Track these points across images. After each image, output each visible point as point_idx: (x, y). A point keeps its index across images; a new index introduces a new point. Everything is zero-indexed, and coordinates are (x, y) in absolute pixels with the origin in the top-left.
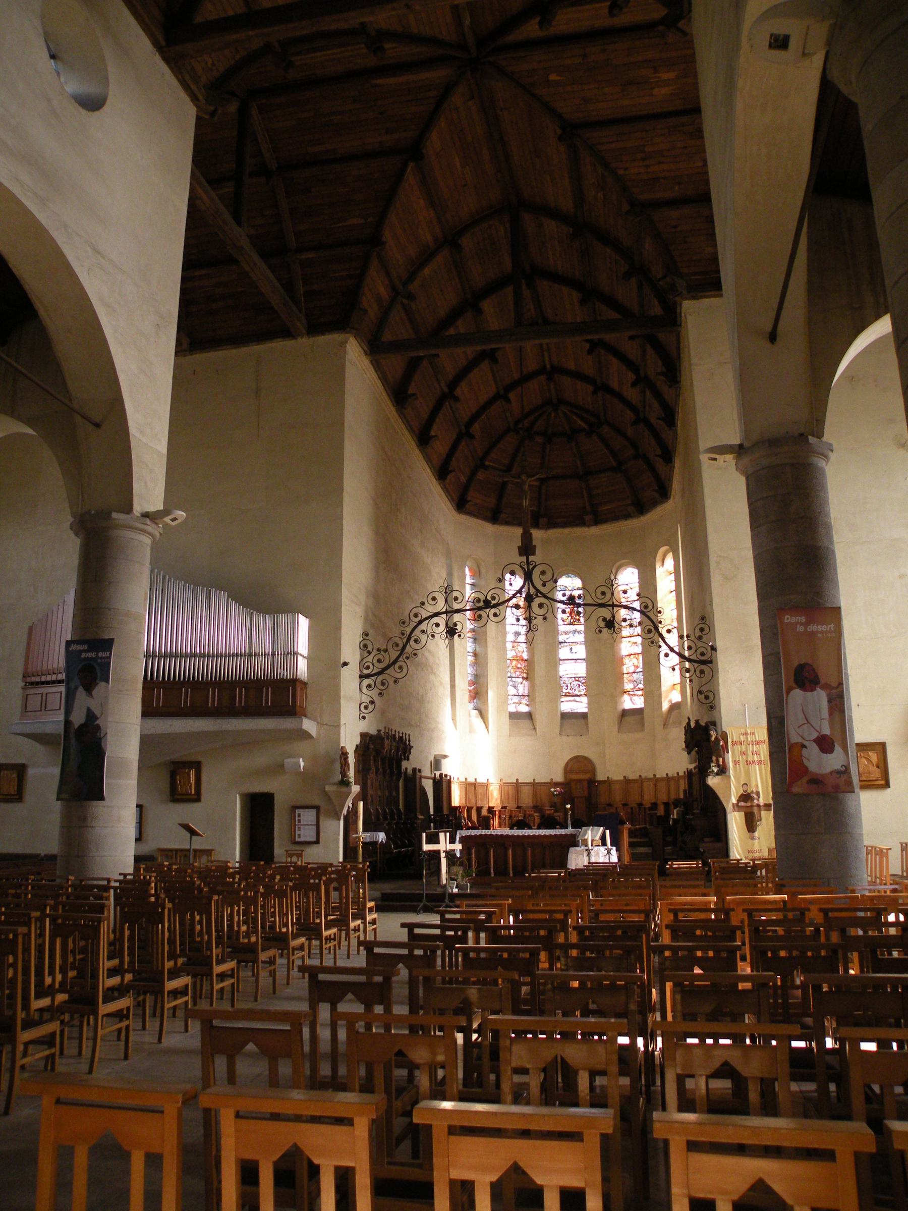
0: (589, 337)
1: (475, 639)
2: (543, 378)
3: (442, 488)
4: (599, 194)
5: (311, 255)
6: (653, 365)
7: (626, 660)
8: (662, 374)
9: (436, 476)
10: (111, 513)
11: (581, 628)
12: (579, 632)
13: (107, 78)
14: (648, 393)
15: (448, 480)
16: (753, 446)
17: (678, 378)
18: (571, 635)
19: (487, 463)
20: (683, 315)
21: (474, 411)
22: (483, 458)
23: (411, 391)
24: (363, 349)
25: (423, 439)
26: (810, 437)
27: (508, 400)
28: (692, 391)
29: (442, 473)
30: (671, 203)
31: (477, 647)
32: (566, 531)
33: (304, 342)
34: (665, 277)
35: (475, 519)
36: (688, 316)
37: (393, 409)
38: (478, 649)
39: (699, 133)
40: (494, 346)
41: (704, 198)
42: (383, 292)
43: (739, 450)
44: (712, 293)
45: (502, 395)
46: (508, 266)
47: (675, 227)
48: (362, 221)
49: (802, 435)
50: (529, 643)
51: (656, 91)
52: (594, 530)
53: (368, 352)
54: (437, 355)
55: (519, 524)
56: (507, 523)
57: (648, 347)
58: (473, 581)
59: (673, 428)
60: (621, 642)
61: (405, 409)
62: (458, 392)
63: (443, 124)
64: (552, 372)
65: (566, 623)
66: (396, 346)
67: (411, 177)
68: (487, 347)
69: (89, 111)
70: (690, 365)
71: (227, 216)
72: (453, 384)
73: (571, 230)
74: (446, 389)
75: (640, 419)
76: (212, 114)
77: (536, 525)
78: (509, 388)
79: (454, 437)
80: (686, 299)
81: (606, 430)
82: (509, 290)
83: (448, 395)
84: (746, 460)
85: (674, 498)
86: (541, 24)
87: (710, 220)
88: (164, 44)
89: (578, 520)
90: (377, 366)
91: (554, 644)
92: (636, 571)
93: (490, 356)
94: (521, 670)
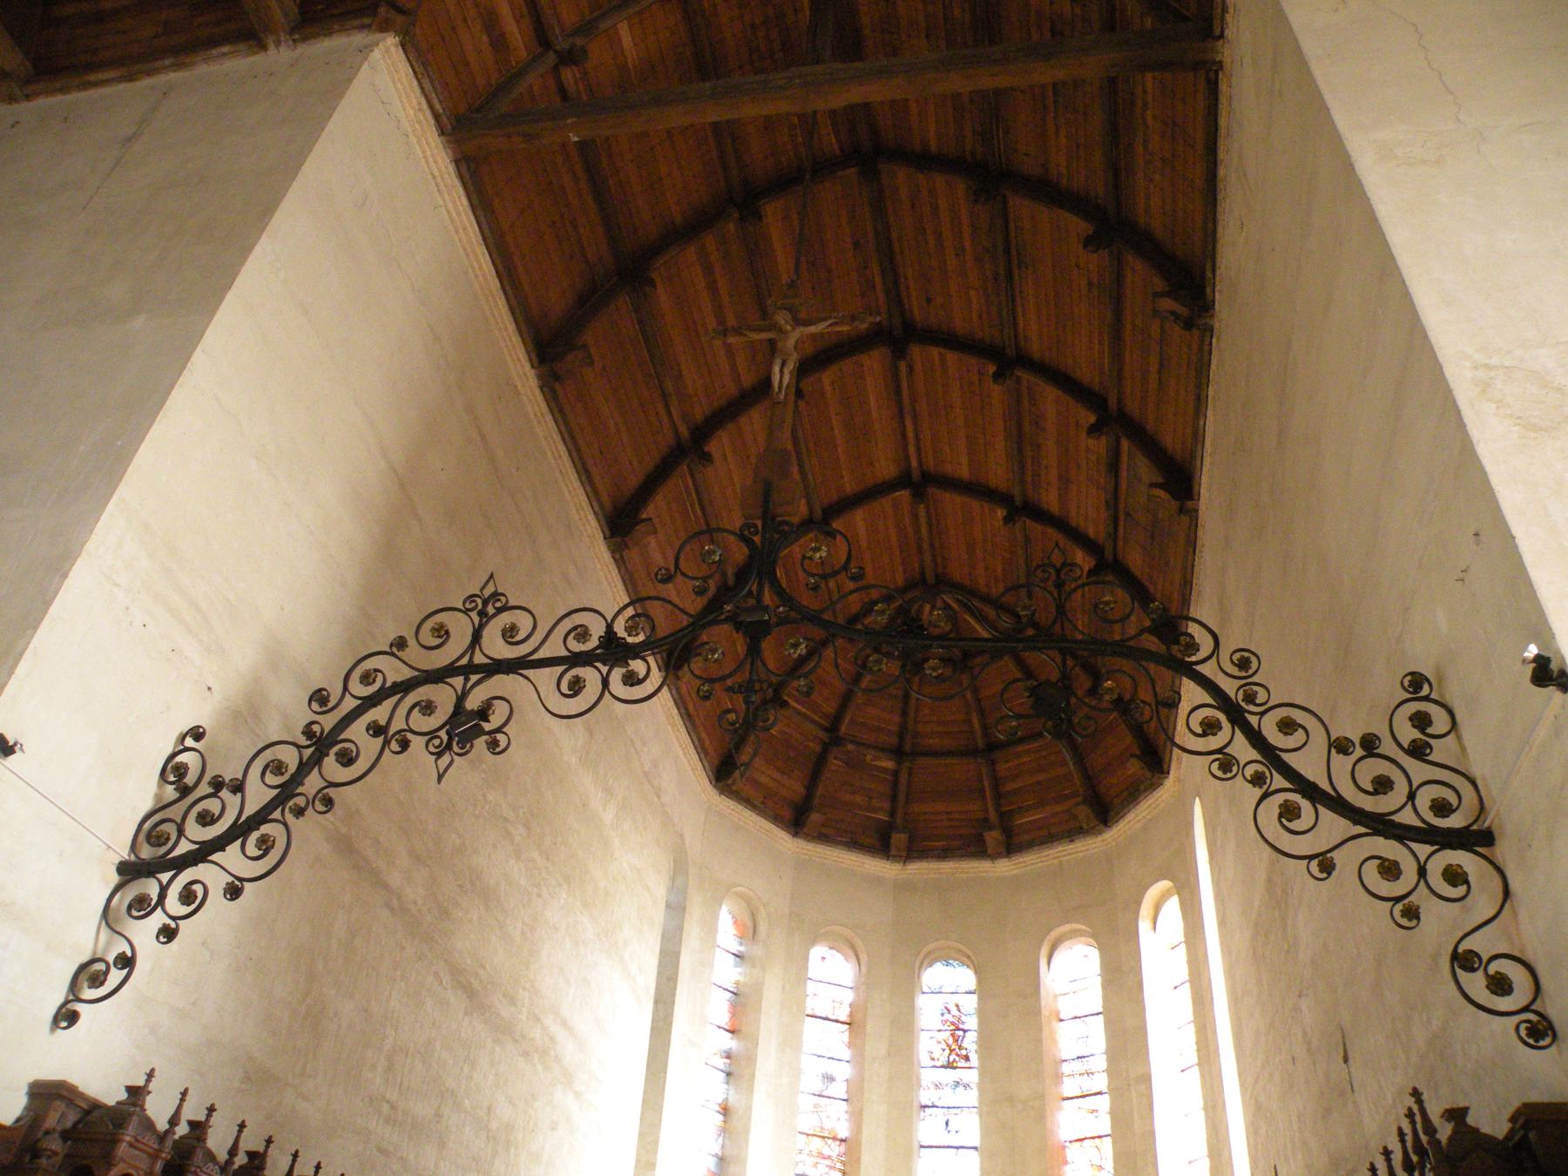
1: (729, 1074)
2: (904, 495)
7: (1072, 1152)
9: (710, 774)
11: (972, 1076)
12: (966, 1086)
18: (948, 1090)
24: (431, 107)
31: (731, 1092)
32: (947, 867)
35: (754, 815)
38: (733, 1099)
50: (855, 1098)
52: (1004, 868)
56: (822, 838)
58: (742, 948)
59: (1190, 503)
60: (1060, 1109)
62: (713, 447)
65: (938, 1064)
89: (972, 845)
91: (907, 1108)
92: (1094, 954)
94: (828, 1162)
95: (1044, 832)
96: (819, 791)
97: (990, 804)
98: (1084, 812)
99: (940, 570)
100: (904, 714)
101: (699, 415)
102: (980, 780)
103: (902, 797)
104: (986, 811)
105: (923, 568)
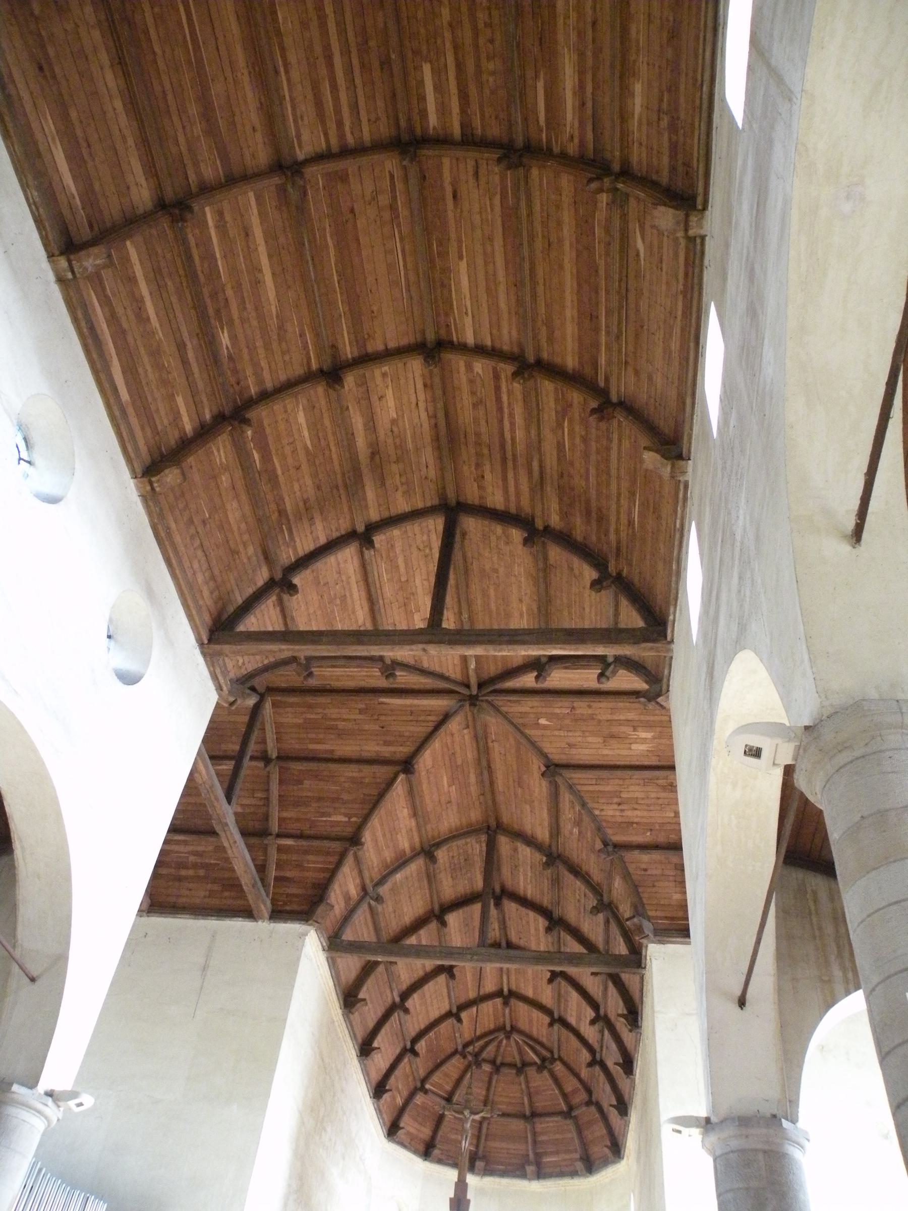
0: (552, 968)
2: (499, 1001)
3: (375, 1110)
4: (574, 830)
5: (289, 842)
6: (614, 1005)
8: (622, 1016)
10: (11, 1084)
13: (149, 661)
14: (606, 1032)
15: (382, 1101)
16: (722, 1122)
17: (639, 1023)
19: (428, 1086)
20: (648, 958)
21: (423, 1026)
22: (423, 1081)
23: (361, 995)
25: (365, 1049)
26: (783, 1120)
27: (460, 1020)
28: (654, 1041)
29: (379, 1090)
30: (644, 847)
32: (505, 1181)
33: (264, 927)
34: (634, 917)
36: (653, 960)
37: (340, 1012)
39: (672, 787)
40: (453, 963)
41: (676, 847)
42: (354, 891)
43: (707, 1124)
44: (678, 939)
45: (454, 1014)
46: (479, 884)
47: (645, 870)
48: (346, 819)
49: (774, 1116)
51: (634, 747)
53: (326, 948)
54: (396, 963)
55: (455, 1165)
56: (440, 1161)
57: (610, 985)
61: (353, 1014)
62: (409, 1004)
63: (437, 745)
64: (508, 996)
66: (355, 947)
67: (399, 787)
68: (446, 963)
69: (125, 684)
70: (653, 1012)
71: (220, 792)
72: (405, 995)
73: (544, 859)
74: (397, 999)
75: (596, 1062)
76: (232, 704)
77: (472, 1168)
78: (463, 1007)
79: (398, 1051)
80: (653, 942)
81: (558, 1067)
82: (477, 908)
83: (399, 1006)
84: (713, 1138)
85: (628, 1159)
86: (537, 678)
87: (681, 868)
88: (206, 642)
90: (332, 964)
93: (449, 971)
95: (558, 1169)
96: (440, 1133)
97: (530, 1147)
98: (579, 1165)
99: (436, 371)
100: (488, 1089)
101: (404, 987)
102: (526, 1132)
103: (483, 1137)
104: (528, 1150)
105: (505, 1021)
